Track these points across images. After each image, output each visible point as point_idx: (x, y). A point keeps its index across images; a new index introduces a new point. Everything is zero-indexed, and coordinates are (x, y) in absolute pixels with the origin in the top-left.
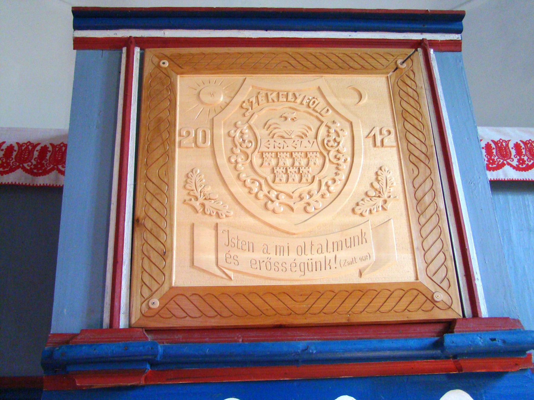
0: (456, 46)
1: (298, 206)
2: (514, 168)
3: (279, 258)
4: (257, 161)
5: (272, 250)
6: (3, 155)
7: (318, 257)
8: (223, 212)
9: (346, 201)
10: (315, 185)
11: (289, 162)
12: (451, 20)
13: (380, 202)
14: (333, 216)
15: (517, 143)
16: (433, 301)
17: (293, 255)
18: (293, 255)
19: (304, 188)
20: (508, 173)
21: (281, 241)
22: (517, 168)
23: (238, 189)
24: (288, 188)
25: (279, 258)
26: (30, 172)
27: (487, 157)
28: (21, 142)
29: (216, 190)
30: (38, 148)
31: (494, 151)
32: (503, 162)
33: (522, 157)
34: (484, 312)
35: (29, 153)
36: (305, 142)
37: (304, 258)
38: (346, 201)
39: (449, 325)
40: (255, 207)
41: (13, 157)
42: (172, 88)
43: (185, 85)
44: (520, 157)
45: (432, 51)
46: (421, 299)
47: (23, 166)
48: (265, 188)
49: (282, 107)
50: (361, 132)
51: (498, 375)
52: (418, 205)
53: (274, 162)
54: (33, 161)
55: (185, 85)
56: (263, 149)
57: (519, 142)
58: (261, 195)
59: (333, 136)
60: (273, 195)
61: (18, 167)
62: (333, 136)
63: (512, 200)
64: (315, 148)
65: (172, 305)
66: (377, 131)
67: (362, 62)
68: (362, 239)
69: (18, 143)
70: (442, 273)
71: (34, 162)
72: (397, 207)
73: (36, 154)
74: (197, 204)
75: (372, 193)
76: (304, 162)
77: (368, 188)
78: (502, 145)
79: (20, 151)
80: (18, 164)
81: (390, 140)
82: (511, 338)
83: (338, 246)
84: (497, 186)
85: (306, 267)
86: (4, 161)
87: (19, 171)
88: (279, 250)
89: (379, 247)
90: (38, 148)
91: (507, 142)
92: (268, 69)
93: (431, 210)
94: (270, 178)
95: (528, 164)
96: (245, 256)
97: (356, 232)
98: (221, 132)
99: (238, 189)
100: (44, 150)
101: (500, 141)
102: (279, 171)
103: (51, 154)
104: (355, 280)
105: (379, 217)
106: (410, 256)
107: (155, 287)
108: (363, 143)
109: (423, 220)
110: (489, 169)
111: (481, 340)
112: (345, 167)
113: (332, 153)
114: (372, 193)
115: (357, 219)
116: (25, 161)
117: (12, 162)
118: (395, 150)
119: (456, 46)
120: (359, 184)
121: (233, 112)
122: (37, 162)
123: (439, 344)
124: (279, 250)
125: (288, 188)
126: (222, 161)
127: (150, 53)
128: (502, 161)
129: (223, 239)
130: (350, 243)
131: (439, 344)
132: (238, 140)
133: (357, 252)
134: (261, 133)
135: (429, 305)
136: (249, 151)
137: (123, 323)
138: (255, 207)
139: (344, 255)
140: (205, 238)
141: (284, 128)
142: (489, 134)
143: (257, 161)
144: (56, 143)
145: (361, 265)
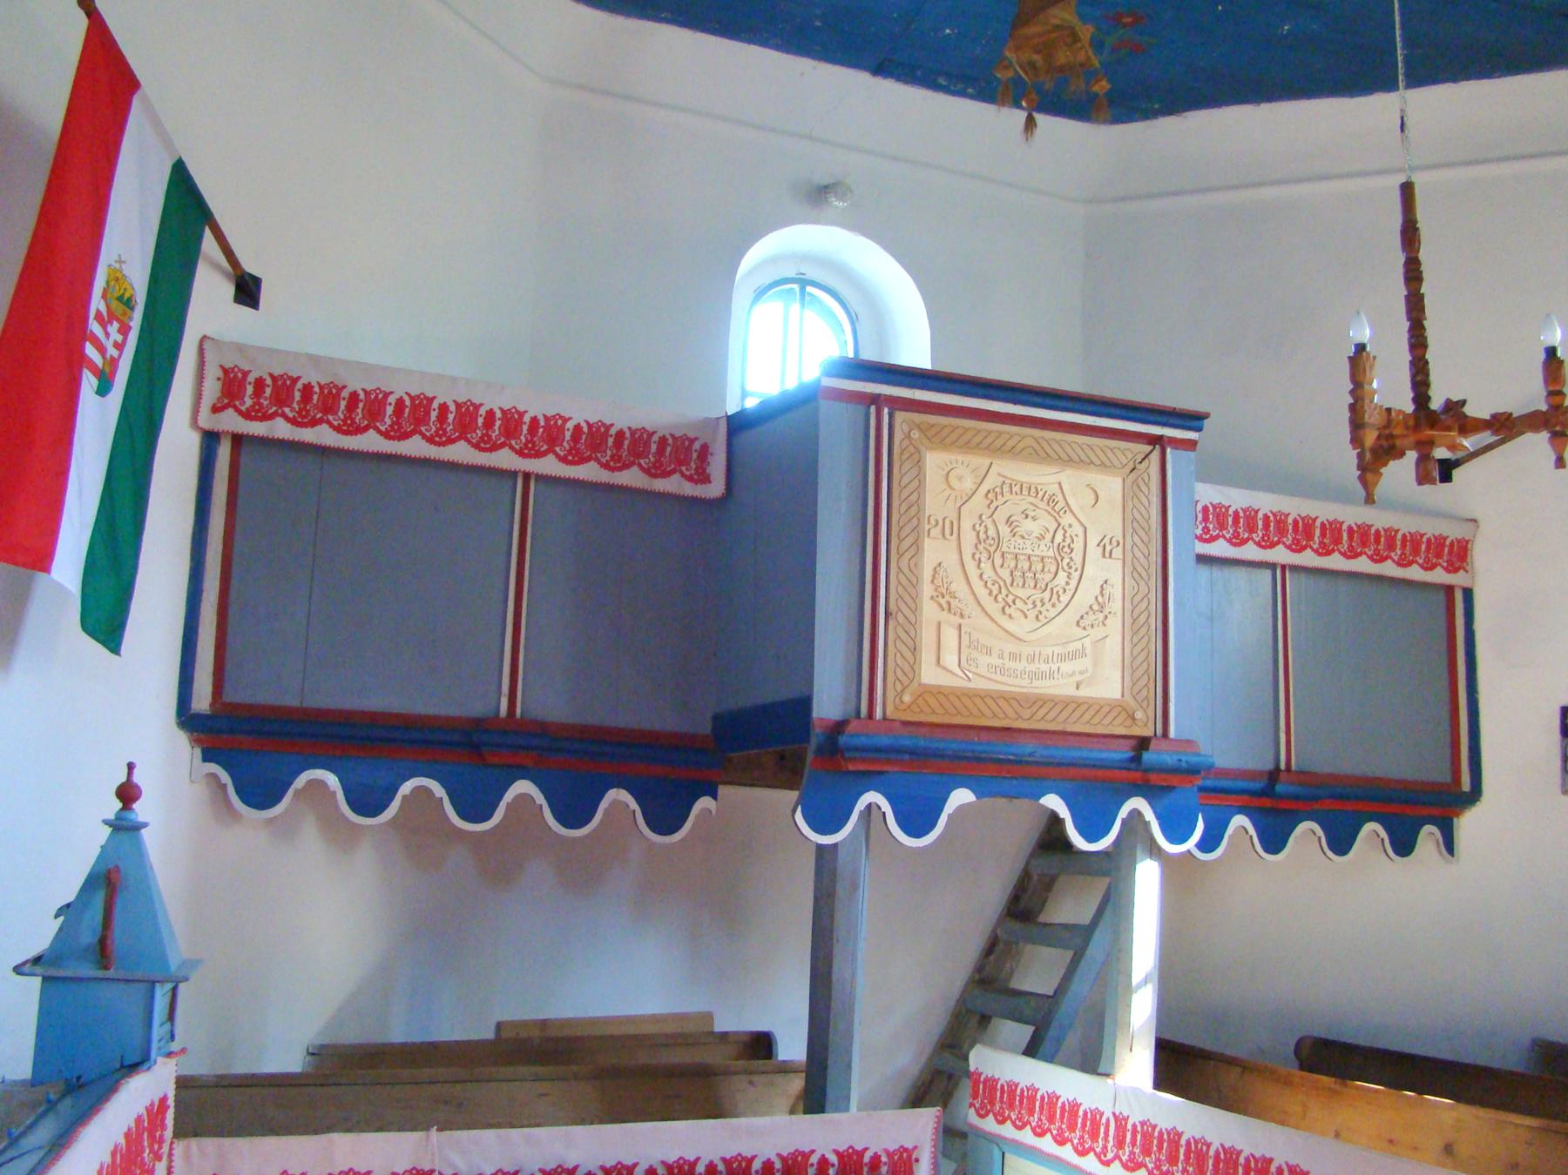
0: (1190, 445)
1: (1032, 614)
3: (1012, 665)
4: (998, 561)
5: (1006, 656)
7: (1044, 667)
8: (966, 613)
9: (1072, 614)
10: (1047, 595)
11: (1026, 565)
12: (1193, 419)
13: (1101, 616)
14: (1062, 625)
16: (1133, 719)
17: (1024, 663)
18: (1024, 663)
19: (1037, 596)
20: (1220, 548)
21: (1010, 647)
23: (981, 591)
24: (1020, 592)
25: (1012, 665)
26: (647, 471)
28: (634, 427)
29: (959, 587)
34: (1172, 733)
36: (1042, 543)
37: (1032, 667)
38: (1072, 614)
39: (1143, 743)
40: (993, 608)
42: (919, 464)
43: (935, 461)
45: (1169, 450)
46: (1124, 715)
48: (1004, 592)
49: (1024, 502)
50: (1093, 541)
51: (1171, 788)
52: (1133, 626)
53: (1013, 564)
55: (935, 461)
56: (1005, 549)
58: (1000, 598)
59: (1068, 540)
60: (1011, 598)
61: (632, 464)
62: (1068, 540)
63: (1217, 573)
64: (1051, 553)
65: (920, 701)
66: (1106, 541)
67: (1104, 459)
68: (1082, 653)
70: (1144, 692)
72: (1115, 624)
73: (654, 447)
74: (943, 602)
75: (1096, 607)
76: (1039, 567)
77: (1093, 601)
81: (1118, 552)
82: (1195, 759)
83: (1064, 658)
84: (1203, 559)
85: (1033, 676)
87: (635, 469)
88: (1014, 657)
89: (1095, 665)
92: (1013, 453)
93: (1144, 630)
94: (1009, 581)
96: (984, 660)
97: (1078, 645)
98: (966, 525)
99: (981, 591)
100: (663, 441)
102: (1018, 574)
104: (1070, 691)
105: (1097, 633)
106: (1119, 674)
107: (906, 682)
108: (1094, 552)
109: (1135, 640)
110: (1200, 538)
111: (1169, 759)
112: (1076, 575)
113: (1066, 560)
114: (1096, 607)
115: (1079, 632)
117: (496, 432)
118: (1120, 563)
119: (1190, 445)
120: (1086, 595)
121: (979, 501)
123: (1136, 759)
124: (1014, 657)
125: (1020, 592)
126: (967, 558)
127: (900, 416)
129: (965, 641)
130: (1073, 656)
131: (1136, 759)
132: (982, 536)
133: (1077, 665)
134: (1005, 530)
135: (1129, 722)
136: (992, 549)
137: (879, 714)
138: (993, 608)
139: (1066, 667)
140: (950, 637)
141: (1027, 526)
142: (1208, 494)
143: (998, 561)
144: (678, 434)
145: (1078, 678)
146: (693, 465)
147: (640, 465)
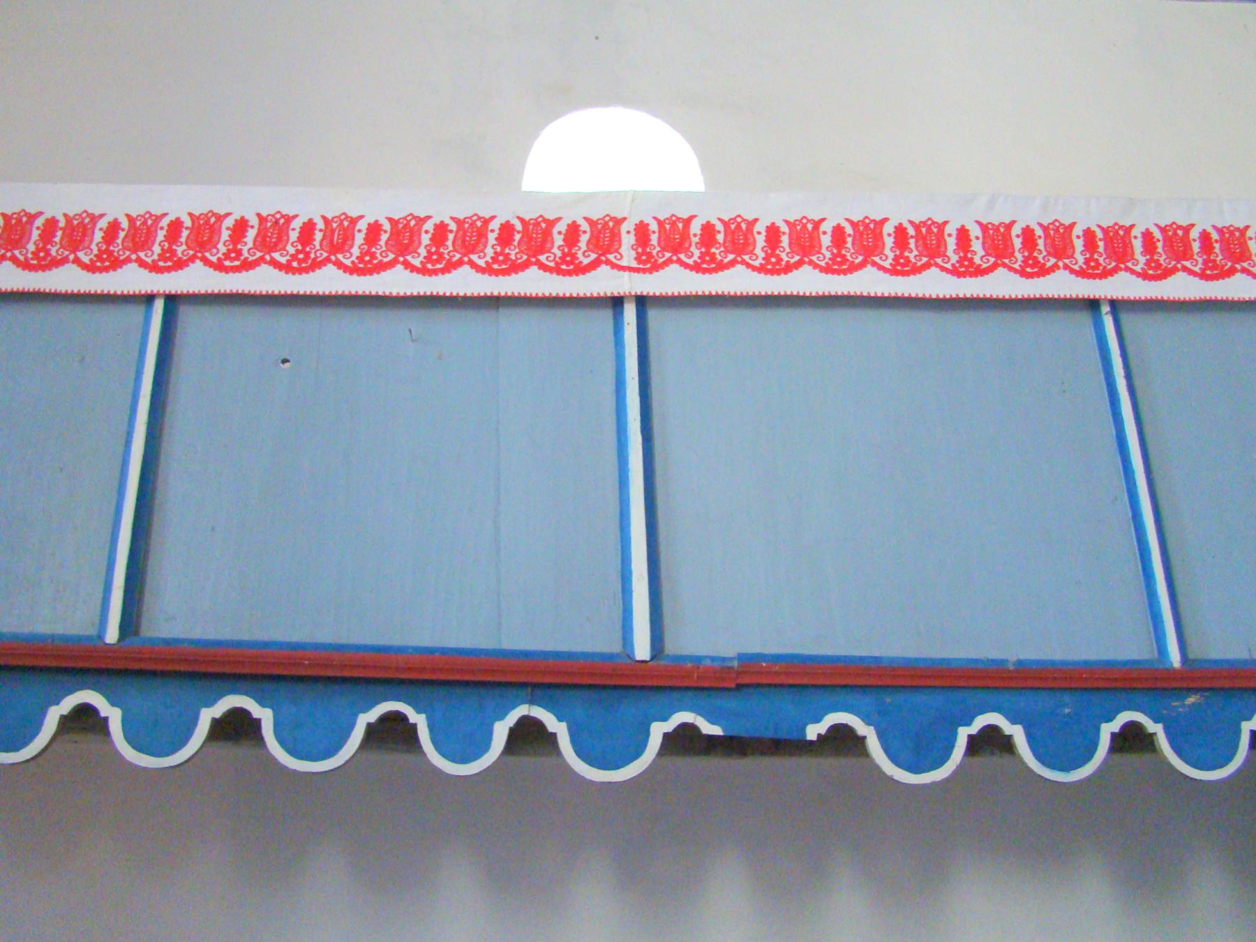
2: (1138, 275)
6: (497, 239)
15: (901, 224)
22: (1144, 276)
27: (831, 251)
30: (39, 222)
31: (1160, 245)
32: (1232, 267)
33: (1096, 256)
35: (745, 235)
41: (183, 240)
44: (902, 253)
47: (272, 258)
54: (555, 250)
57: (1094, 228)
69: (65, 215)
71: (291, 250)
78: (1175, 234)
79: (794, 236)
80: (191, 252)
86: (434, 250)
87: (330, 269)
90: (39, 222)
91: (1187, 229)
95: (246, 259)
101: (1175, 227)
103: (126, 236)
116: (542, 249)
122: (563, 253)
128: (1229, 264)
146: (157, 249)
147: (937, 265)
